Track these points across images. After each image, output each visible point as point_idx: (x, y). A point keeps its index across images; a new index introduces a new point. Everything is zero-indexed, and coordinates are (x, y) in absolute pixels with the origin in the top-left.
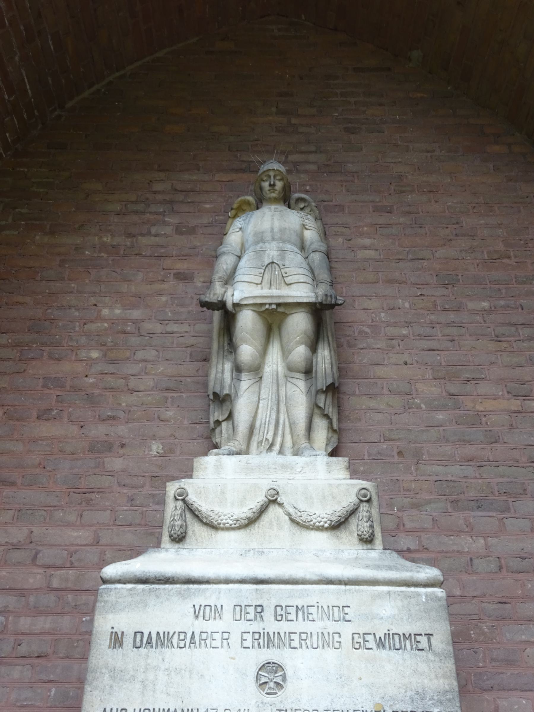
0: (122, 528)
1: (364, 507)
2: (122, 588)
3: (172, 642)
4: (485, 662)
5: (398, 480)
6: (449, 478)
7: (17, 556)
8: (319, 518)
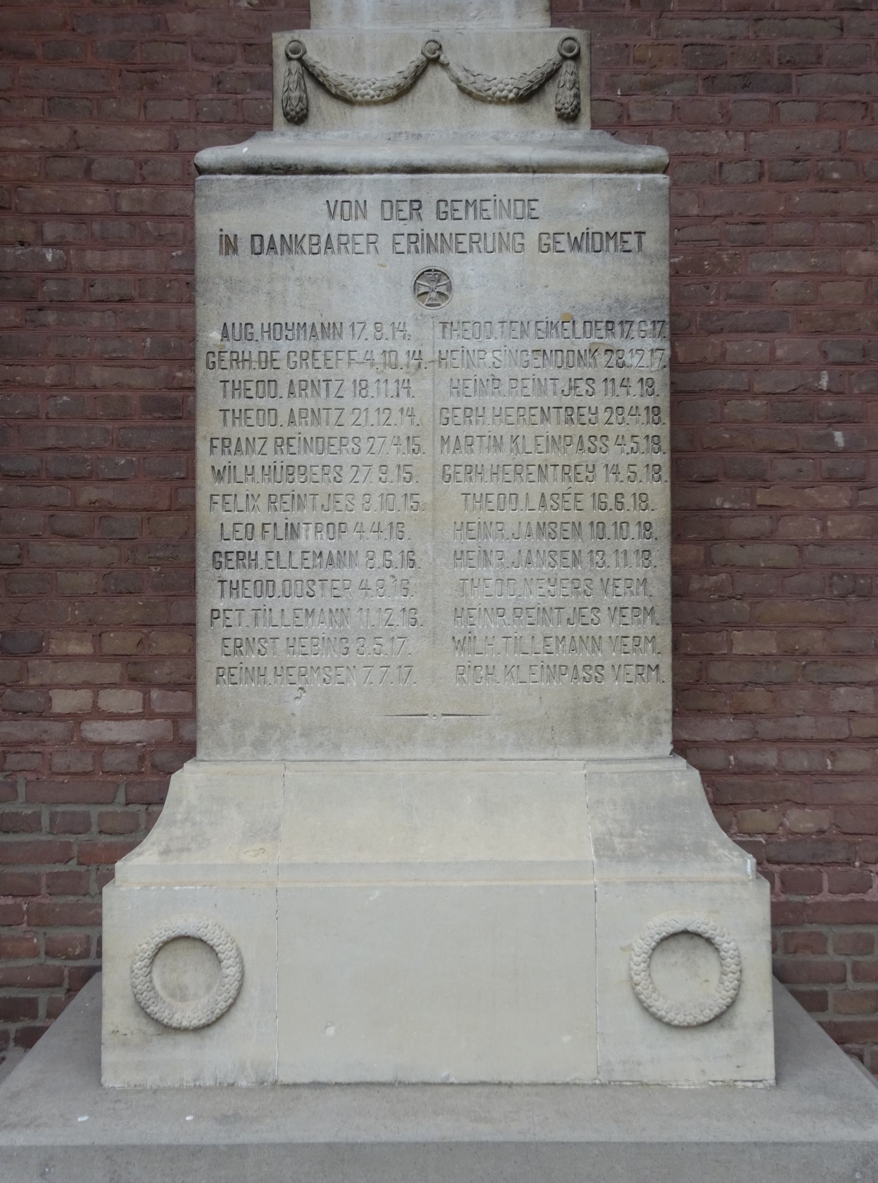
0: (209, 127)
1: (569, 66)
2: (227, 179)
3: (301, 247)
4: (717, 299)
5: (627, 46)
6: (707, 39)
7: (60, 166)
8: (500, 85)
